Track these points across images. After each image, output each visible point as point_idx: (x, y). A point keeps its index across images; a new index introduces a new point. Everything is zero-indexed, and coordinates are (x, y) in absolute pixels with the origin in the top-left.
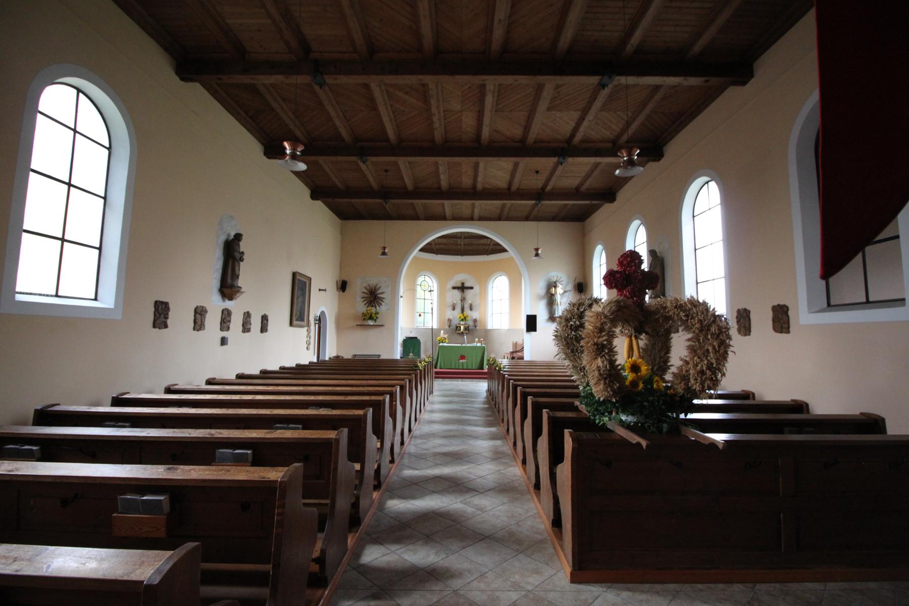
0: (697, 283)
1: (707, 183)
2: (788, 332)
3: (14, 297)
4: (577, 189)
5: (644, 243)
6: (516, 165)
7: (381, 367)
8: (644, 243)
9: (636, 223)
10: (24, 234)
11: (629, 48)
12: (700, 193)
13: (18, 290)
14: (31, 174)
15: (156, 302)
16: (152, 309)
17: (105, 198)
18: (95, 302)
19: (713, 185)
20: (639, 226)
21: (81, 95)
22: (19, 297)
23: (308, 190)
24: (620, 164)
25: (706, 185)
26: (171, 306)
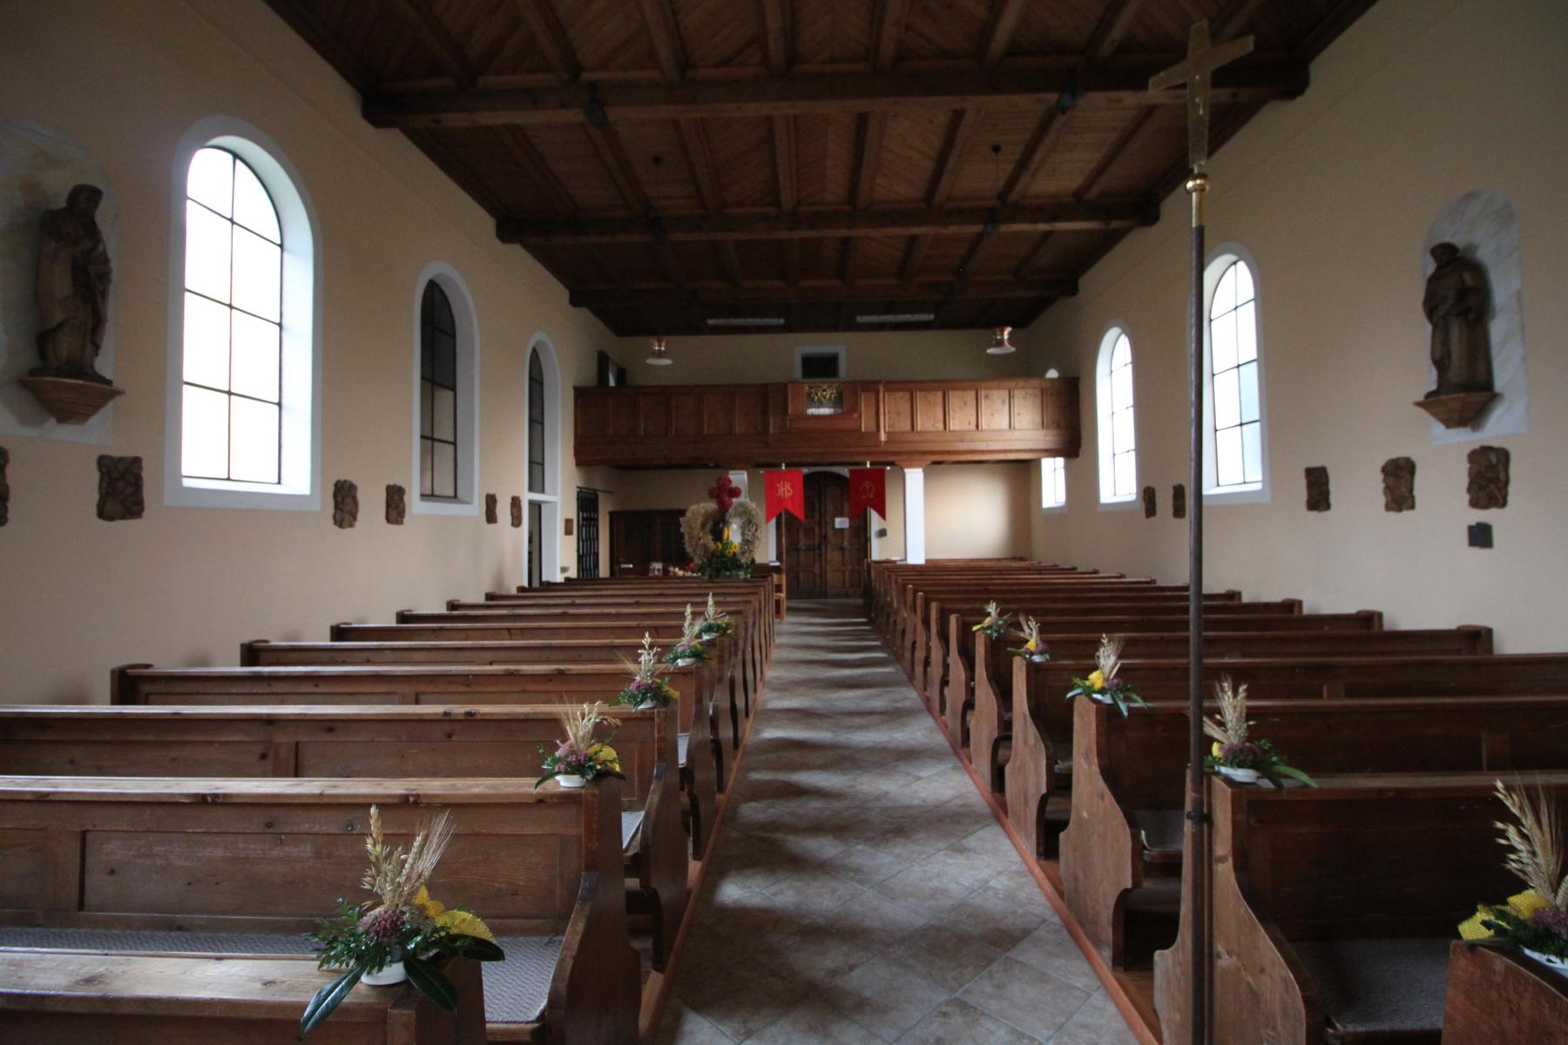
0: (1216, 430)
1: (1235, 263)
2: (1412, 507)
3: (181, 482)
4: (1079, 195)
5: (1126, 365)
6: (958, 116)
7: (983, 452)
8: (1126, 365)
9: (1113, 333)
10: (185, 387)
11: (1107, 48)
12: (1223, 279)
13: (184, 472)
14: (187, 294)
15: (388, 488)
16: (95, 476)
17: (280, 325)
18: (278, 486)
19: (1242, 265)
20: (1227, 270)
21: (238, 162)
22: (187, 483)
23: (492, 219)
24: (670, 680)
25: (1233, 267)
26: (497, 498)
